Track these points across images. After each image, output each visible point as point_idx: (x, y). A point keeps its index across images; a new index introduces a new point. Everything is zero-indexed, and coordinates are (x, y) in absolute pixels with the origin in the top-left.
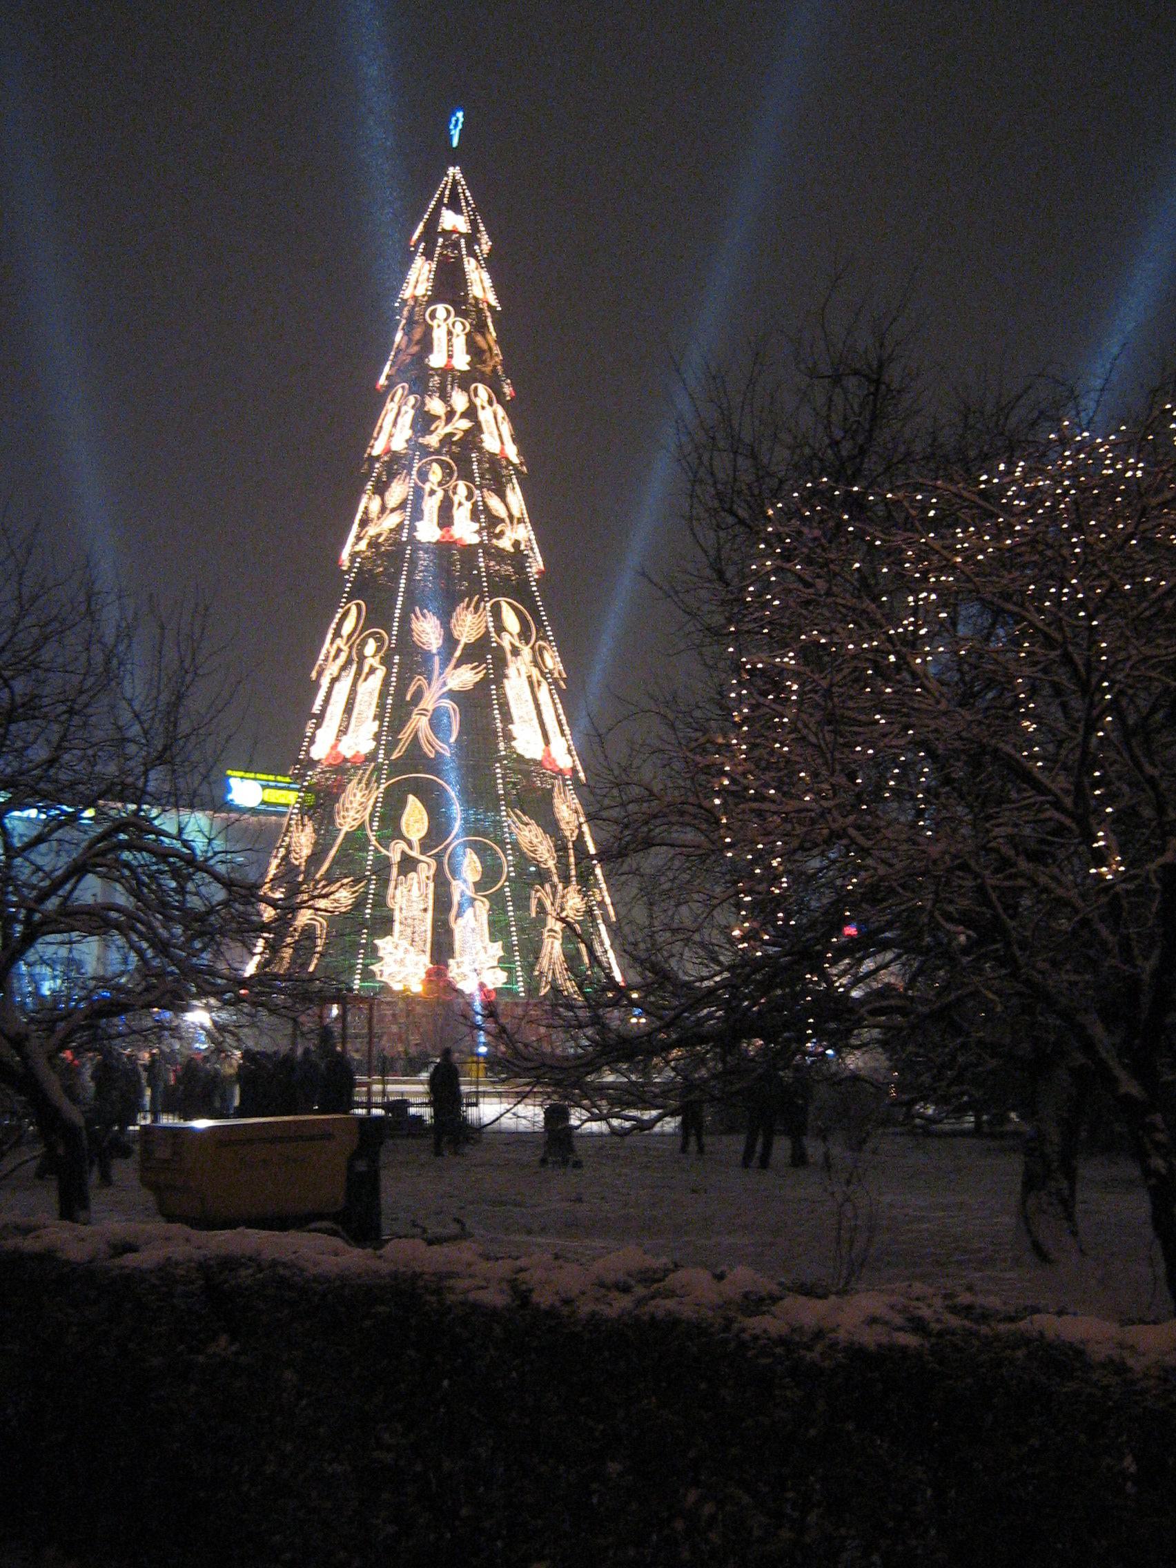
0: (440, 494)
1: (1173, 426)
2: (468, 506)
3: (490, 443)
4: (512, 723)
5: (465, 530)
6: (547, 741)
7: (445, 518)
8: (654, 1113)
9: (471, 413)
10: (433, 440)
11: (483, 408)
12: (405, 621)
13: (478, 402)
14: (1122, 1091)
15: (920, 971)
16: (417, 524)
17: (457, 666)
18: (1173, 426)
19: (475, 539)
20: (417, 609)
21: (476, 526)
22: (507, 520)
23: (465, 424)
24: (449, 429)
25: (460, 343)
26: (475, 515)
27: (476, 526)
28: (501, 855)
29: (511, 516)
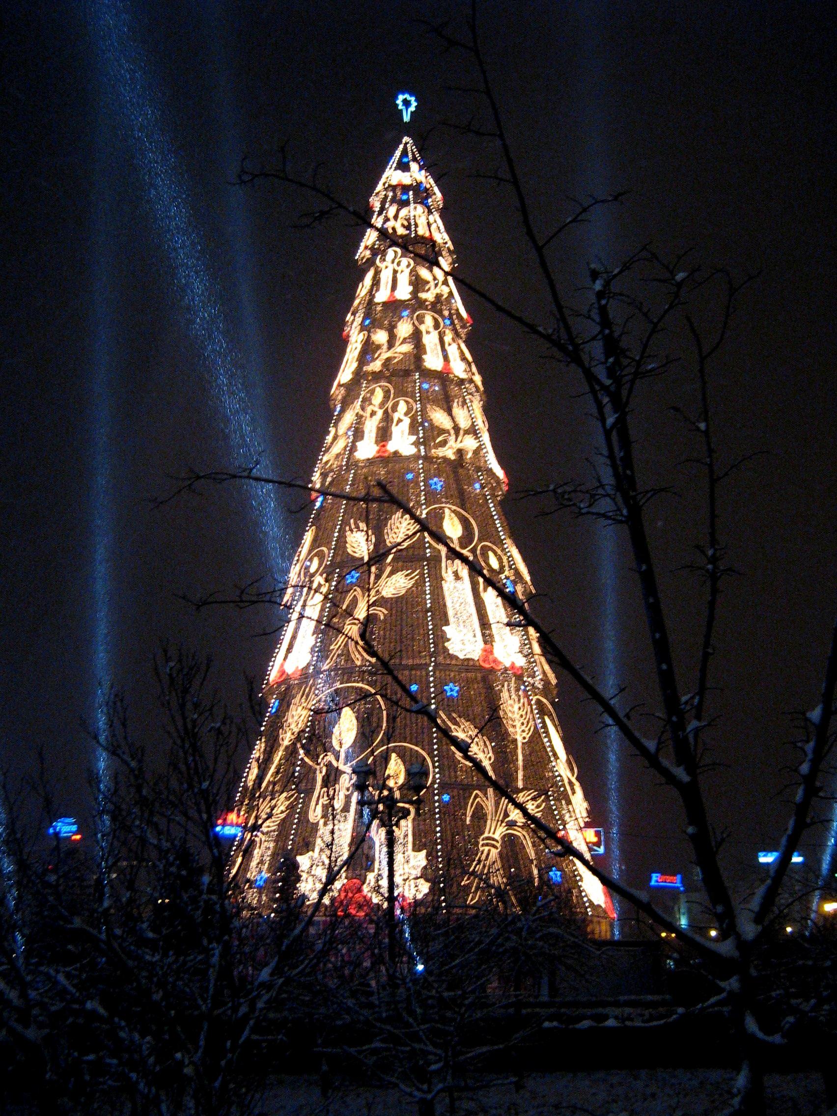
0: (380, 413)
1: (829, 907)
2: (407, 421)
3: (433, 361)
4: (447, 623)
5: (402, 442)
6: (488, 639)
7: (384, 435)
8: (327, 483)
9: (416, 337)
10: (376, 366)
11: (428, 332)
12: (342, 532)
13: (423, 328)
14: (299, 859)
15: (57, 847)
16: (358, 444)
17: (392, 573)
18: (829, 907)
19: (412, 450)
20: (352, 521)
21: (413, 438)
22: (452, 432)
23: (407, 348)
24: (389, 354)
25: (404, 280)
26: (413, 429)
27: (413, 438)
28: (428, 760)
29: (457, 429)
